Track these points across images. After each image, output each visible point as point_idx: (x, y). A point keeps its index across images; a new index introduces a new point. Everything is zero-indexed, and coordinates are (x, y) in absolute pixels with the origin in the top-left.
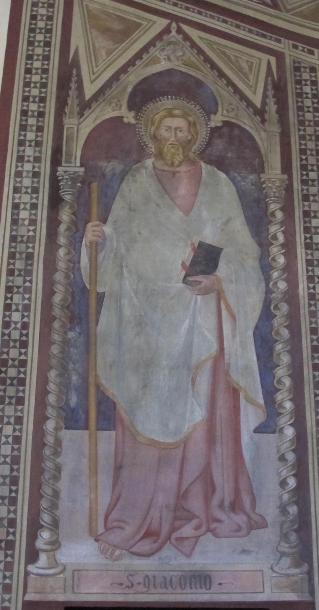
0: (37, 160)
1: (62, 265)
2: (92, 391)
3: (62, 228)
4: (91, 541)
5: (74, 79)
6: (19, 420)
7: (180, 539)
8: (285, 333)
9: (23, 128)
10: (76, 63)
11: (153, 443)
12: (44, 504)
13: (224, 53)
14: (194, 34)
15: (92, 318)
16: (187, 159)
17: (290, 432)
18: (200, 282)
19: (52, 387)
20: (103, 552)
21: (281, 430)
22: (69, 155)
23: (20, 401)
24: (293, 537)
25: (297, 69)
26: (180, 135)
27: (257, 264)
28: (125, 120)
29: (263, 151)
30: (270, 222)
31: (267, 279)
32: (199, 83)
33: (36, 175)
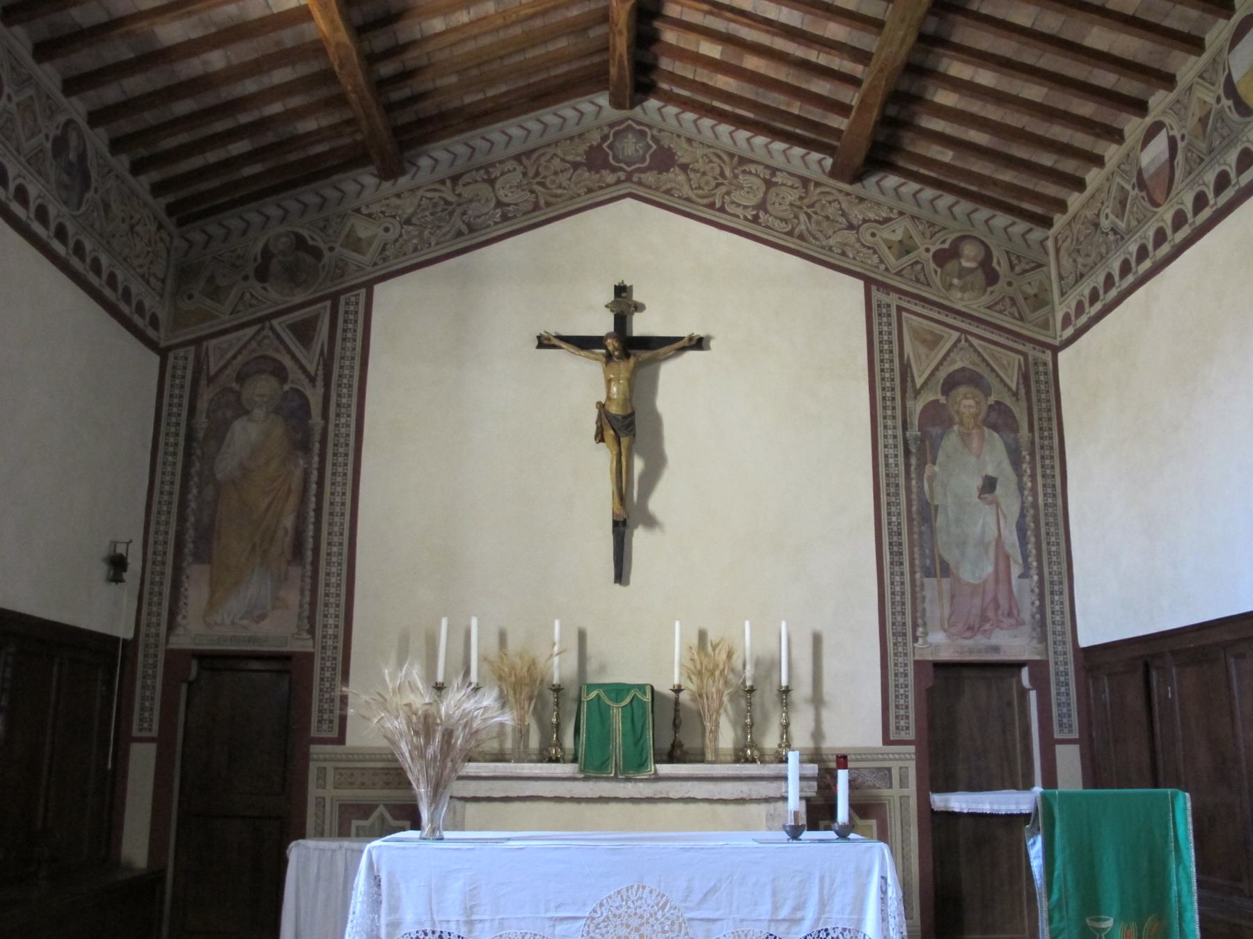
0: (895, 428)
1: (914, 490)
2: (937, 557)
3: (913, 468)
4: (942, 632)
5: (909, 375)
6: (902, 574)
7: (985, 631)
8: (1032, 525)
9: (885, 408)
10: (909, 365)
11: (968, 584)
12: (919, 614)
13: (993, 355)
14: (975, 342)
15: (933, 519)
16: (977, 426)
17: (1036, 578)
18: (986, 498)
19: (917, 556)
20: (948, 637)
21: (1032, 577)
22: (912, 424)
23: (901, 564)
24: (1038, 629)
25: (1036, 364)
26: (972, 410)
27: (1016, 487)
28: (941, 402)
29: (1017, 418)
30: (1023, 462)
31: (1022, 495)
32: (981, 377)
33: (895, 437)
